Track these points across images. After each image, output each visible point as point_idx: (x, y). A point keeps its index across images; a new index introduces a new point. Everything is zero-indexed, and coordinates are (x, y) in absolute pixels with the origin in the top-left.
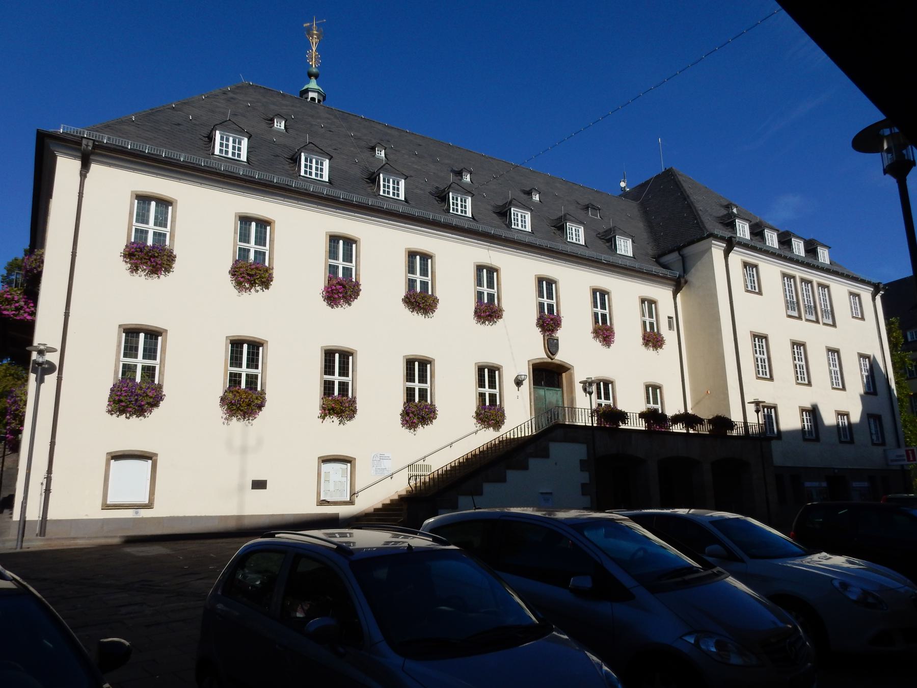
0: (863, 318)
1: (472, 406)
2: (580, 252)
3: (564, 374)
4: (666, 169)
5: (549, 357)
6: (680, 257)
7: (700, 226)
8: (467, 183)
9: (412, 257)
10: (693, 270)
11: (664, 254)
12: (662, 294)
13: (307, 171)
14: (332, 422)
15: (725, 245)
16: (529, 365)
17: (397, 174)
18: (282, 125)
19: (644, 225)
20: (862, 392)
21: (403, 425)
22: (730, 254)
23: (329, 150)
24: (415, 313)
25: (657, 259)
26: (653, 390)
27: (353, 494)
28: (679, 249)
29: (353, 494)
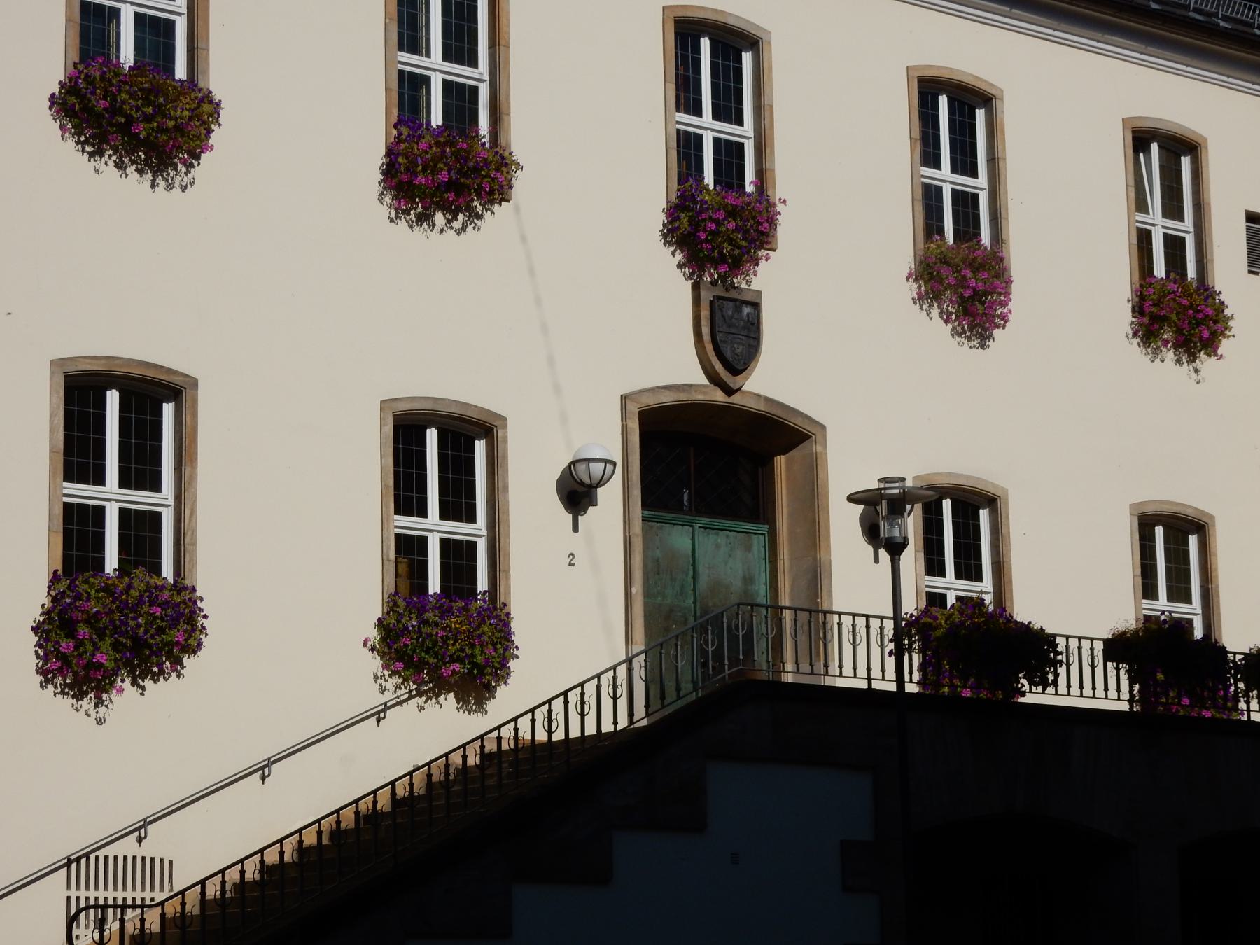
3: (781, 462)
5: (714, 379)
21: (47, 676)
24: (107, 166)
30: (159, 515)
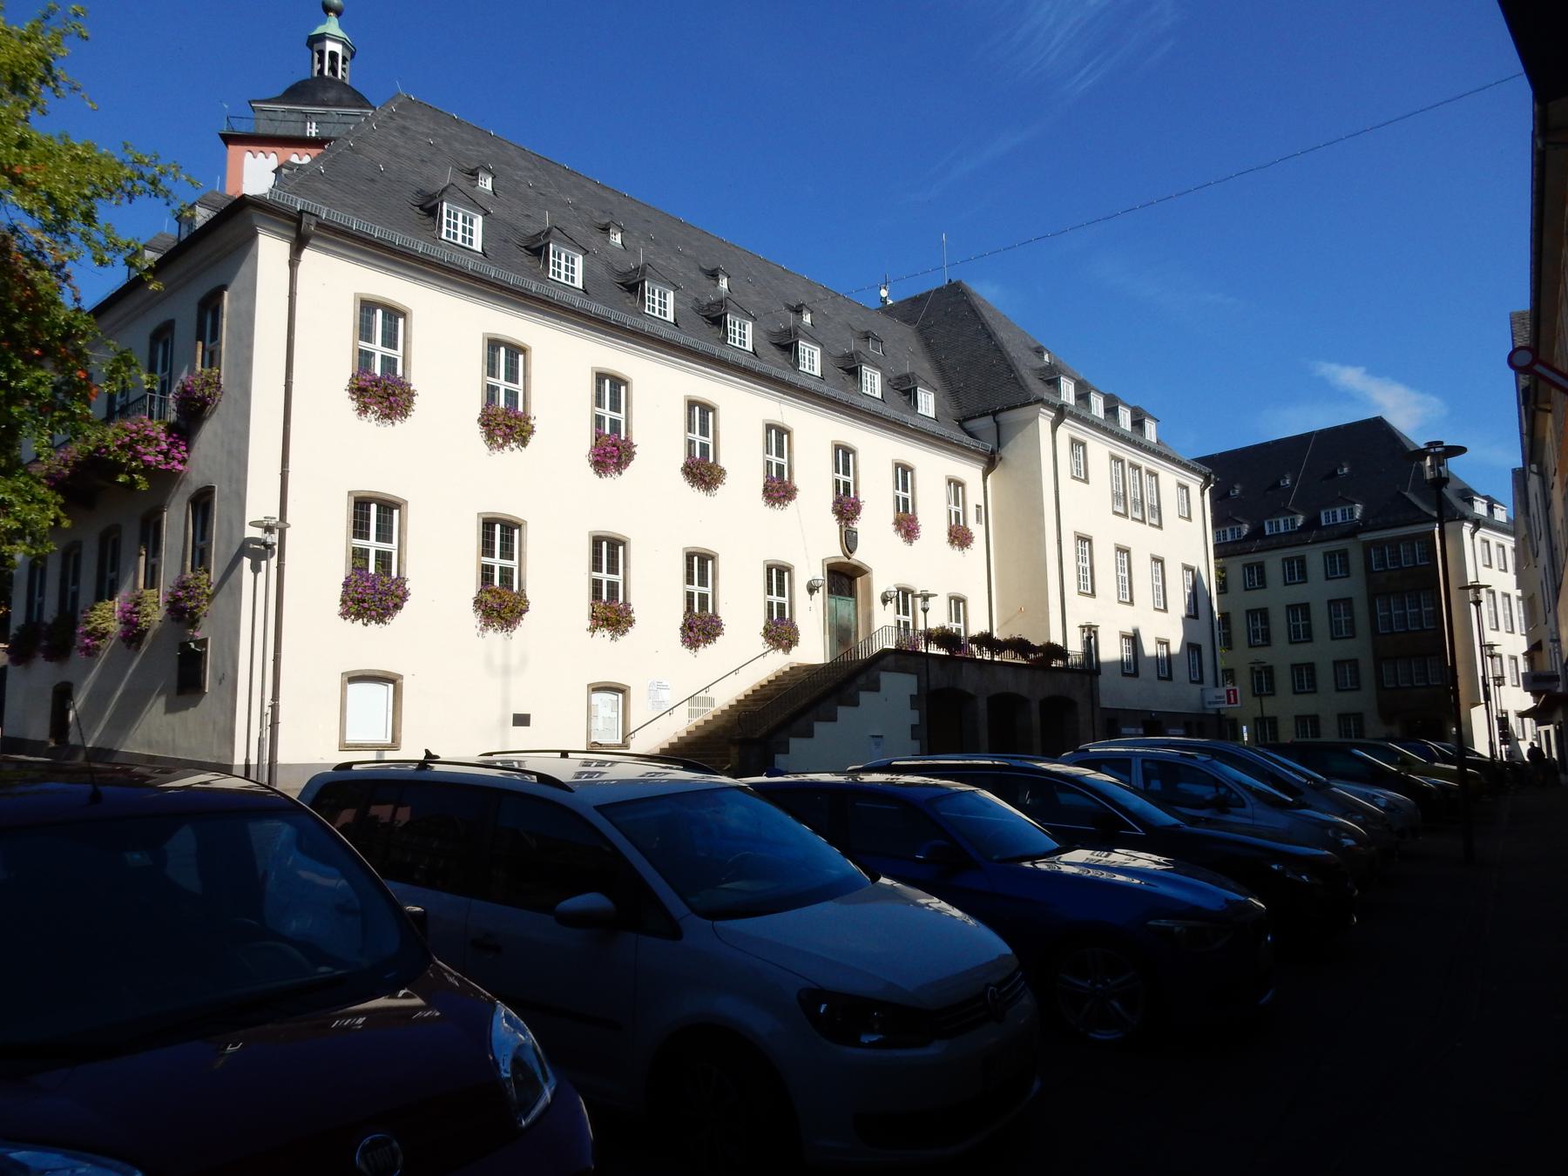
0: (1189, 518)
1: (470, 585)
2: (665, 333)
3: (859, 579)
4: (950, 281)
5: (845, 555)
6: (995, 424)
7: (1017, 382)
8: (483, 193)
9: (368, 311)
10: (1010, 444)
11: (967, 419)
12: (970, 472)
13: (450, 232)
14: (604, 635)
15: (1054, 415)
16: (823, 566)
17: (665, 282)
18: (487, 183)
19: (932, 367)
20: (1184, 616)
21: (684, 642)
22: (1059, 428)
23: (820, 338)
24: (695, 488)
25: (961, 423)
26: (958, 603)
27: (626, 736)
28: (995, 414)
29: (626, 736)
30: (513, 569)
